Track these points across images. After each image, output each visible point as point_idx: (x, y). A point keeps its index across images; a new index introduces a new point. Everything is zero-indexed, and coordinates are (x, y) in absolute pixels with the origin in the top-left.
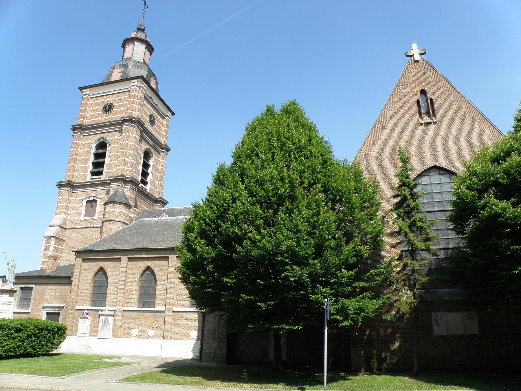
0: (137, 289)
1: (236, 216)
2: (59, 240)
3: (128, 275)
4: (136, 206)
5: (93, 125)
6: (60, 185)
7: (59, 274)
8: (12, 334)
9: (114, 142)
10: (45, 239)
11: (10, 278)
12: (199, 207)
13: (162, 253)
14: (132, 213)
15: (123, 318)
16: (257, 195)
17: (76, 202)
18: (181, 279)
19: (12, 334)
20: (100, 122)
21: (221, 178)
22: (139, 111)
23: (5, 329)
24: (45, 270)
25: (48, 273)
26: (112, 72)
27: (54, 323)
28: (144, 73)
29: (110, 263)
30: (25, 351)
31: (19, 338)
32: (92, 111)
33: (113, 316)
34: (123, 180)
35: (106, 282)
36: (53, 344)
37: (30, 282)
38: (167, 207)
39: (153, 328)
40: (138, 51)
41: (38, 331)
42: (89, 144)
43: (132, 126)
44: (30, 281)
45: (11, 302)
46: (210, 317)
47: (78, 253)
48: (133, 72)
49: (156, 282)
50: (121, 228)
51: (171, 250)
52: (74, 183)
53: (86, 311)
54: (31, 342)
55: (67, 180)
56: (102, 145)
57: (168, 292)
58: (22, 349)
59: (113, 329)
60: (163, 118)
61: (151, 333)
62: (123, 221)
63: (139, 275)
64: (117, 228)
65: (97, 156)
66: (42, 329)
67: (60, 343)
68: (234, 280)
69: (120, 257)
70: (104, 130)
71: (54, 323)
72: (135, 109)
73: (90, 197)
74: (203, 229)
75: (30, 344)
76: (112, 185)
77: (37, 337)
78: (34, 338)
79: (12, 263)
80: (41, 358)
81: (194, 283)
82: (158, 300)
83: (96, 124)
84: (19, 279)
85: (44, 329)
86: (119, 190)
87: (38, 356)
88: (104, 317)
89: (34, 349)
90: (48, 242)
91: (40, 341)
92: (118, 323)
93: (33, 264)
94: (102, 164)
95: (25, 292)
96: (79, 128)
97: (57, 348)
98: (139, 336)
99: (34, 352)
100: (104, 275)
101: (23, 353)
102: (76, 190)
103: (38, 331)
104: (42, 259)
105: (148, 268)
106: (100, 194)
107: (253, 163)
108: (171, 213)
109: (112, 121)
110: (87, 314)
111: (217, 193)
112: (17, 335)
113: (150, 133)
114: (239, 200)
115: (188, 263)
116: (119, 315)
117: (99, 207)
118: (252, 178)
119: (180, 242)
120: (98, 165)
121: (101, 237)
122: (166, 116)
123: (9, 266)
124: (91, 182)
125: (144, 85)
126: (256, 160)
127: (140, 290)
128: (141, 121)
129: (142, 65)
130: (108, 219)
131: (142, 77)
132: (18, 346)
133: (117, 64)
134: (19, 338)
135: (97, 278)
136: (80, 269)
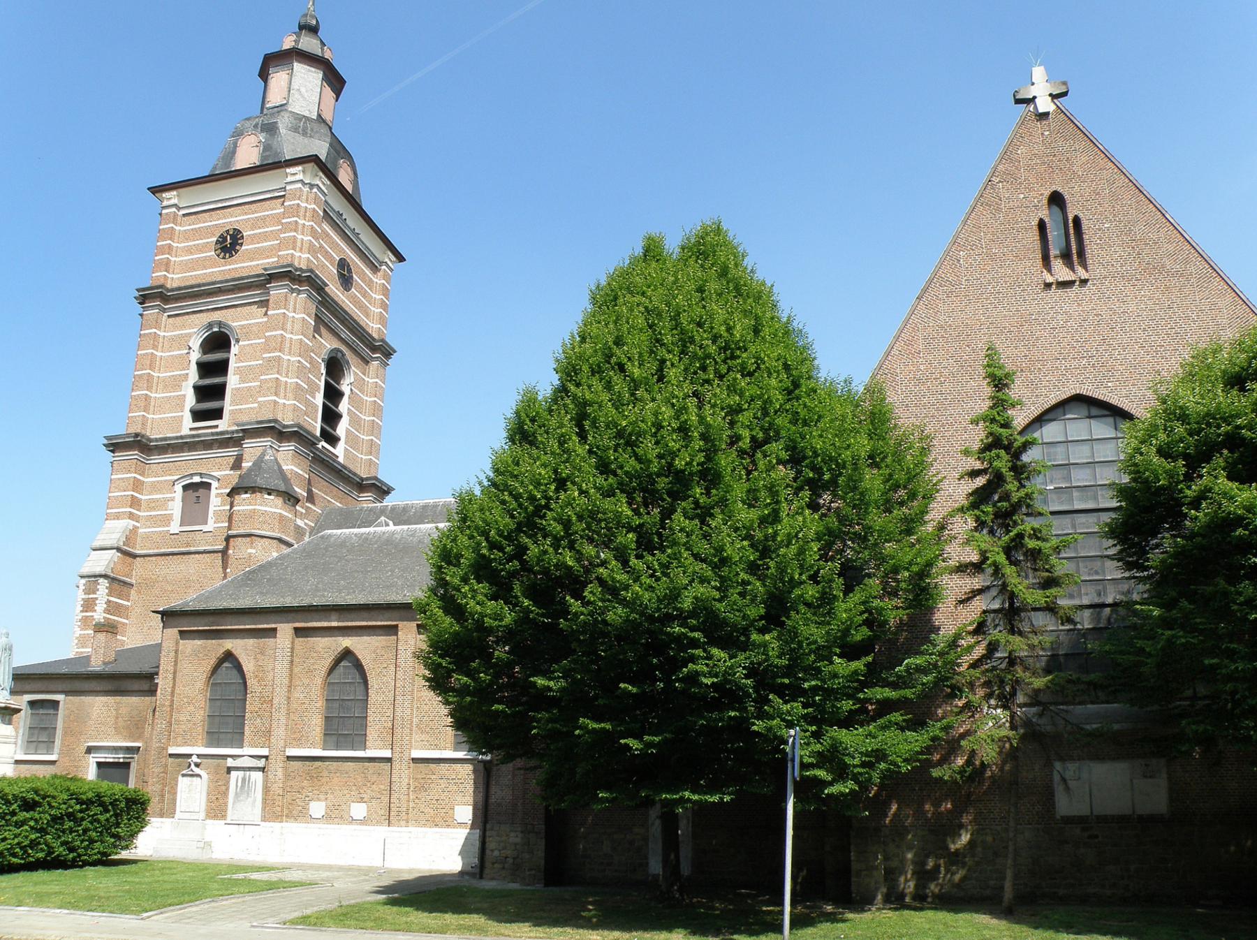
0: (318, 705)
2: (118, 584)
3: (296, 670)
4: (311, 498)
6: (115, 446)
8: (14, 813)
10: (83, 581)
12: (470, 500)
13: (382, 616)
14: (302, 516)
15: (287, 776)
16: (619, 471)
18: (428, 680)
19: (14, 813)
22: (312, 249)
24: (88, 658)
25: (96, 665)
26: (235, 146)
28: (321, 148)
30: (50, 853)
31: (32, 823)
32: (189, 251)
33: (263, 769)
34: (278, 433)
36: (117, 837)
38: (389, 501)
39: (362, 800)
40: (301, 89)
41: (78, 807)
42: (184, 337)
43: (292, 291)
44: (52, 686)
45: (7, 737)
46: (506, 772)
47: (169, 616)
48: (292, 145)
49: (367, 689)
50: (275, 555)
52: (151, 440)
53: (195, 759)
54: (64, 831)
55: (132, 430)
56: (218, 341)
57: (399, 713)
58: (42, 850)
60: (375, 269)
61: (358, 810)
62: (279, 535)
63: (324, 672)
65: (205, 369)
66: (89, 802)
67: (133, 835)
69: (273, 626)
70: (221, 300)
71: (118, 787)
75: (59, 837)
76: (248, 443)
77: (78, 822)
78: (68, 824)
81: (462, 691)
82: (372, 733)
83: (199, 286)
84: (23, 679)
85: (93, 803)
86: (267, 457)
87: (81, 867)
88: (241, 774)
89: (72, 850)
90: (91, 589)
91: (85, 831)
92: (276, 788)
93: (59, 641)
94: (217, 392)
95: (41, 711)
97: (127, 847)
98: (328, 818)
99: (71, 856)
100: (235, 672)
101: (45, 859)
102: (156, 459)
103: (78, 807)
104: (78, 632)
106: (218, 469)
110: (197, 765)
111: (517, 464)
112: (28, 815)
114: (574, 483)
115: (446, 641)
117: (216, 500)
119: (425, 588)
120: (210, 395)
121: (225, 577)
122: (381, 263)
124: (193, 436)
125: (322, 181)
128: (317, 276)
129: (316, 126)
130: (242, 531)
131: (314, 159)
132: (32, 841)
133: (248, 124)
136: (176, 657)
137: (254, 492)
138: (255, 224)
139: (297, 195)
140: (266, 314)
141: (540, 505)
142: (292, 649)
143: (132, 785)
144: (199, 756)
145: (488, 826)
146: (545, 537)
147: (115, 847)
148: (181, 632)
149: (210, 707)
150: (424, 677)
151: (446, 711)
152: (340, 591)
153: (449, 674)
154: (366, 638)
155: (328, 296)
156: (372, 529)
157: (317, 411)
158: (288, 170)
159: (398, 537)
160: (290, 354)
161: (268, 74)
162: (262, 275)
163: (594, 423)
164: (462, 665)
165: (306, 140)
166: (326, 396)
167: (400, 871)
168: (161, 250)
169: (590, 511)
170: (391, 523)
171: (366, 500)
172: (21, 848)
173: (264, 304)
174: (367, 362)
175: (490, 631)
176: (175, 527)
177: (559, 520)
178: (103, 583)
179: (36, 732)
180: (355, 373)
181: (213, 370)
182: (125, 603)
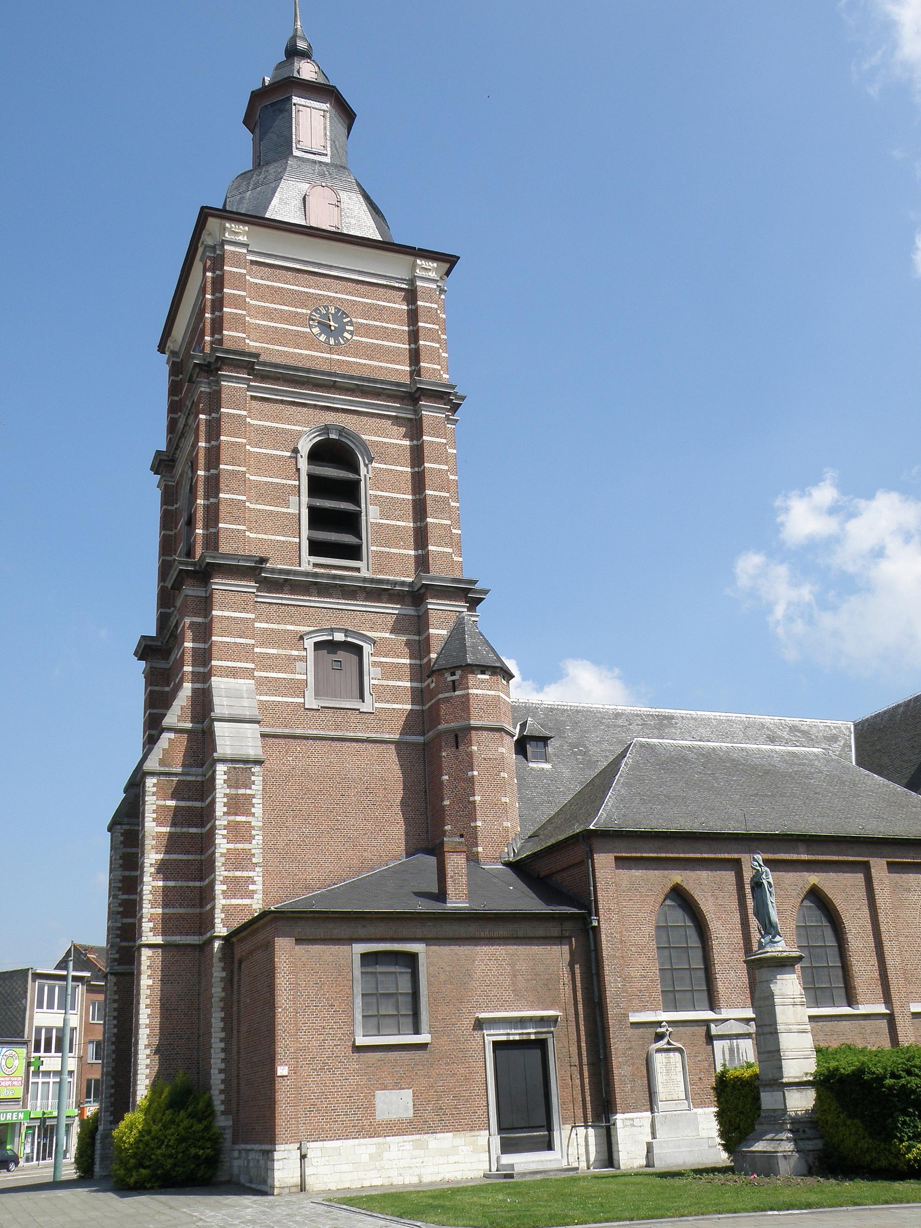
20: (325, 368)
69: (736, 856)
73: (332, 630)
83: (308, 371)
88: (726, 1043)
95: (380, 969)
124: (315, 575)
138: (368, 311)
154: (832, 875)
158: (419, 262)
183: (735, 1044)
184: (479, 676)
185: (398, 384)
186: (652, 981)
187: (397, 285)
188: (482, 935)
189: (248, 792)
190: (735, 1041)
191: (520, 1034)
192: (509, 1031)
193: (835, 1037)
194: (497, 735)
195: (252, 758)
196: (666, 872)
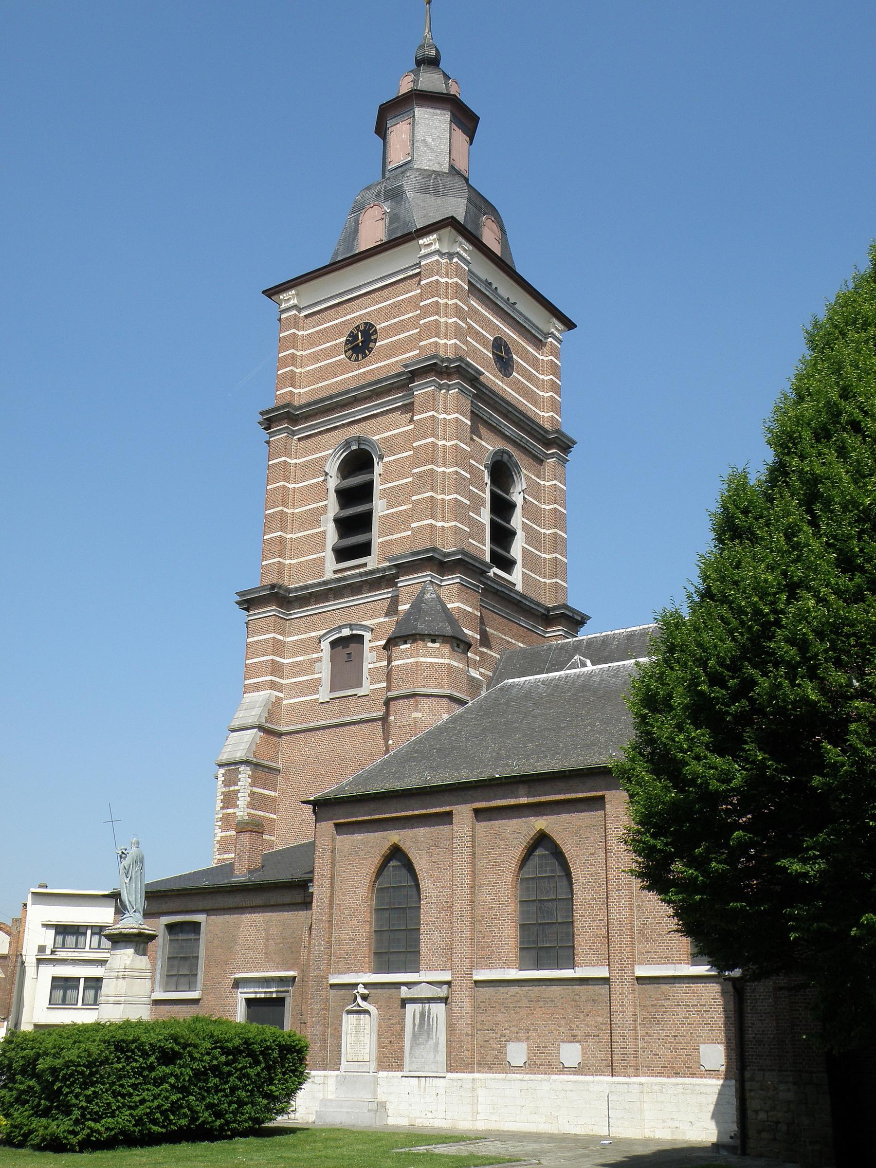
0: (510, 909)
1: (803, 645)
2: (262, 770)
3: (479, 865)
4: (485, 640)
5: (322, 400)
6: (248, 603)
7: (271, 876)
8: (151, 1068)
9: (393, 445)
10: (222, 771)
11: (134, 897)
12: (677, 625)
13: (580, 786)
14: (476, 665)
15: (477, 1008)
16: (867, 566)
17: (301, 647)
18: (640, 875)
19: (151, 1068)
21: (740, 520)
22: (459, 333)
23: (133, 1052)
24: (232, 865)
25: (240, 875)
26: (357, 223)
27: (270, 1030)
28: (457, 206)
29: (422, 832)
30: (193, 1120)
31: (172, 1080)
32: (315, 358)
33: (445, 1000)
34: (438, 563)
35: (414, 892)
36: (270, 1097)
37: (191, 906)
38: (584, 635)
39: (573, 1039)
40: (428, 137)
41: (223, 1058)
42: (318, 462)
43: (440, 387)
44: (191, 904)
45: (141, 970)
46: (762, 992)
47: (322, 807)
48: (422, 209)
49: (571, 884)
50: (445, 717)
51: (599, 775)
52: (290, 591)
53: (361, 990)
54: (208, 1091)
55: (267, 582)
56: (359, 461)
57: (614, 916)
58: (185, 1116)
59: (449, 1042)
60: (539, 344)
61: (571, 1054)
62: (447, 692)
63: (514, 865)
64: (429, 716)
65: (346, 496)
66: (236, 1052)
67: (290, 1094)
68: (821, 865)
69: (448, 809)
70: (358, 411)
71: (270, 1030)
72: (443, 329)
73: (340, 628)
74: (702, 693)
75: (204, 1098)
76: (403, 582)
77: (224, 1077)
78: (213, 1081)
79: (133, 852)
80: (240, 1143)
81: (686, 886)
82: (582, 943)
83: (331, 397)
84: (158, 898)
85: (240, 1052)
86: (428, 596)
87: (230, 1138)
88: (418, 1007)
89: (218, 1115)
90: (231, 780)
91: (233, 1089)
92: (463, 1025)
93: (197, 848)
94: (363, 522)
95: (181, 937)
96: (281, 418)
97: (282, 1111)
98: (532, 1066)
99: (218, 1123)
100: (404, 872)
101: (188, 1126)
102: (297, 613)
103: (223, 1058)
104: (220, 834)
105: (542, 839)
106: (371, 616)
107: (842, 452)
108: (599, 651)
109: (380, 381)
110: (365, 998)
111: (737, 567)
112: (167, 1071)
113: (503, 399)
114: (809, 589)
115: (659, 814)
116: (463, 999)
117: (371, 657)
118: (845, 509)
119: (627, 746)
120: (354, 526)
121: (387, 751)
122: (547, 335)
123: (126, 862)
124: (339, 580)
125: (463, 248)
126: (851, 440)
127: (522, 913)
128: (469, 365)
129: (448, 181)
130: (404, 691)
131: (451, 222)
132: (173, 1103)
133: (369, 194)
134: (172, 1080)
135: (384, 882)
136: (333, 859)
137: (414, 641)
138: (388, 313)
139: (435, 269)
140: (412, 420)
141: (769, 622)
142: (473, 837)
143: (287, 1028)
144: (366, 985)
145: (747, 1075)
146: (776, 665)
147: (269, 1110)
148: (336, 825)
149: (377, 920)
150: (632, 871)
151: (671, 911)
152: (527, 757)
153: (669, 859)
154: (564, 817)
155: (485, 386)
156: (562, 673)
157: (484, 530)
158: (421, 242)
159: (597, 679)
160: (444, 465)
161: (386, 129)
162: (403, 373)
163: (827, 503)
164: (683, 848)
165: (439, 201)
166: (494, 510)
167: (630, 1142)
168: (284, 362)
169: (833, 625)
170: (588, 662)
171: (556, 636)
172: (163, 1113)
173: (408, 408)
174: (541, 462)
175: (724, 797)
176: (324, 694)
177: (791, 641)
178: (245, 772)
179: (176, 962)
180: (527, 477)
181: (355, 496)
182: (273, 794)
183: (427, 1008)
184: (402, 647)
185: (398, 375)
186: (359, 944)
187: (411, 273)
188: (244, 905)
189: (236, 788)
190: (427, 1005)
191: (265, 992)
192: (257, 990)
193: (541, 1004)
194: (412, 700)
195: (237, 760)
196: (385, 833)
